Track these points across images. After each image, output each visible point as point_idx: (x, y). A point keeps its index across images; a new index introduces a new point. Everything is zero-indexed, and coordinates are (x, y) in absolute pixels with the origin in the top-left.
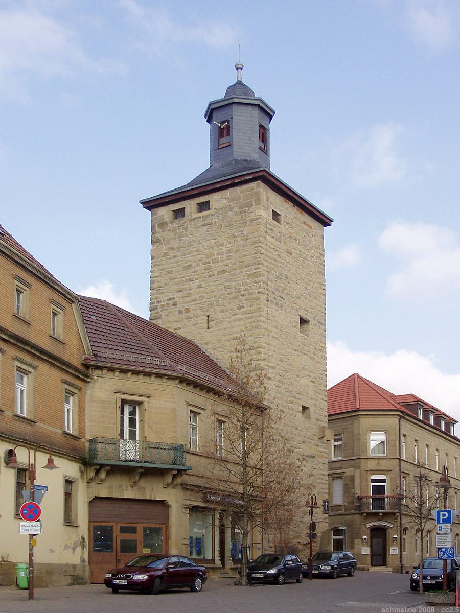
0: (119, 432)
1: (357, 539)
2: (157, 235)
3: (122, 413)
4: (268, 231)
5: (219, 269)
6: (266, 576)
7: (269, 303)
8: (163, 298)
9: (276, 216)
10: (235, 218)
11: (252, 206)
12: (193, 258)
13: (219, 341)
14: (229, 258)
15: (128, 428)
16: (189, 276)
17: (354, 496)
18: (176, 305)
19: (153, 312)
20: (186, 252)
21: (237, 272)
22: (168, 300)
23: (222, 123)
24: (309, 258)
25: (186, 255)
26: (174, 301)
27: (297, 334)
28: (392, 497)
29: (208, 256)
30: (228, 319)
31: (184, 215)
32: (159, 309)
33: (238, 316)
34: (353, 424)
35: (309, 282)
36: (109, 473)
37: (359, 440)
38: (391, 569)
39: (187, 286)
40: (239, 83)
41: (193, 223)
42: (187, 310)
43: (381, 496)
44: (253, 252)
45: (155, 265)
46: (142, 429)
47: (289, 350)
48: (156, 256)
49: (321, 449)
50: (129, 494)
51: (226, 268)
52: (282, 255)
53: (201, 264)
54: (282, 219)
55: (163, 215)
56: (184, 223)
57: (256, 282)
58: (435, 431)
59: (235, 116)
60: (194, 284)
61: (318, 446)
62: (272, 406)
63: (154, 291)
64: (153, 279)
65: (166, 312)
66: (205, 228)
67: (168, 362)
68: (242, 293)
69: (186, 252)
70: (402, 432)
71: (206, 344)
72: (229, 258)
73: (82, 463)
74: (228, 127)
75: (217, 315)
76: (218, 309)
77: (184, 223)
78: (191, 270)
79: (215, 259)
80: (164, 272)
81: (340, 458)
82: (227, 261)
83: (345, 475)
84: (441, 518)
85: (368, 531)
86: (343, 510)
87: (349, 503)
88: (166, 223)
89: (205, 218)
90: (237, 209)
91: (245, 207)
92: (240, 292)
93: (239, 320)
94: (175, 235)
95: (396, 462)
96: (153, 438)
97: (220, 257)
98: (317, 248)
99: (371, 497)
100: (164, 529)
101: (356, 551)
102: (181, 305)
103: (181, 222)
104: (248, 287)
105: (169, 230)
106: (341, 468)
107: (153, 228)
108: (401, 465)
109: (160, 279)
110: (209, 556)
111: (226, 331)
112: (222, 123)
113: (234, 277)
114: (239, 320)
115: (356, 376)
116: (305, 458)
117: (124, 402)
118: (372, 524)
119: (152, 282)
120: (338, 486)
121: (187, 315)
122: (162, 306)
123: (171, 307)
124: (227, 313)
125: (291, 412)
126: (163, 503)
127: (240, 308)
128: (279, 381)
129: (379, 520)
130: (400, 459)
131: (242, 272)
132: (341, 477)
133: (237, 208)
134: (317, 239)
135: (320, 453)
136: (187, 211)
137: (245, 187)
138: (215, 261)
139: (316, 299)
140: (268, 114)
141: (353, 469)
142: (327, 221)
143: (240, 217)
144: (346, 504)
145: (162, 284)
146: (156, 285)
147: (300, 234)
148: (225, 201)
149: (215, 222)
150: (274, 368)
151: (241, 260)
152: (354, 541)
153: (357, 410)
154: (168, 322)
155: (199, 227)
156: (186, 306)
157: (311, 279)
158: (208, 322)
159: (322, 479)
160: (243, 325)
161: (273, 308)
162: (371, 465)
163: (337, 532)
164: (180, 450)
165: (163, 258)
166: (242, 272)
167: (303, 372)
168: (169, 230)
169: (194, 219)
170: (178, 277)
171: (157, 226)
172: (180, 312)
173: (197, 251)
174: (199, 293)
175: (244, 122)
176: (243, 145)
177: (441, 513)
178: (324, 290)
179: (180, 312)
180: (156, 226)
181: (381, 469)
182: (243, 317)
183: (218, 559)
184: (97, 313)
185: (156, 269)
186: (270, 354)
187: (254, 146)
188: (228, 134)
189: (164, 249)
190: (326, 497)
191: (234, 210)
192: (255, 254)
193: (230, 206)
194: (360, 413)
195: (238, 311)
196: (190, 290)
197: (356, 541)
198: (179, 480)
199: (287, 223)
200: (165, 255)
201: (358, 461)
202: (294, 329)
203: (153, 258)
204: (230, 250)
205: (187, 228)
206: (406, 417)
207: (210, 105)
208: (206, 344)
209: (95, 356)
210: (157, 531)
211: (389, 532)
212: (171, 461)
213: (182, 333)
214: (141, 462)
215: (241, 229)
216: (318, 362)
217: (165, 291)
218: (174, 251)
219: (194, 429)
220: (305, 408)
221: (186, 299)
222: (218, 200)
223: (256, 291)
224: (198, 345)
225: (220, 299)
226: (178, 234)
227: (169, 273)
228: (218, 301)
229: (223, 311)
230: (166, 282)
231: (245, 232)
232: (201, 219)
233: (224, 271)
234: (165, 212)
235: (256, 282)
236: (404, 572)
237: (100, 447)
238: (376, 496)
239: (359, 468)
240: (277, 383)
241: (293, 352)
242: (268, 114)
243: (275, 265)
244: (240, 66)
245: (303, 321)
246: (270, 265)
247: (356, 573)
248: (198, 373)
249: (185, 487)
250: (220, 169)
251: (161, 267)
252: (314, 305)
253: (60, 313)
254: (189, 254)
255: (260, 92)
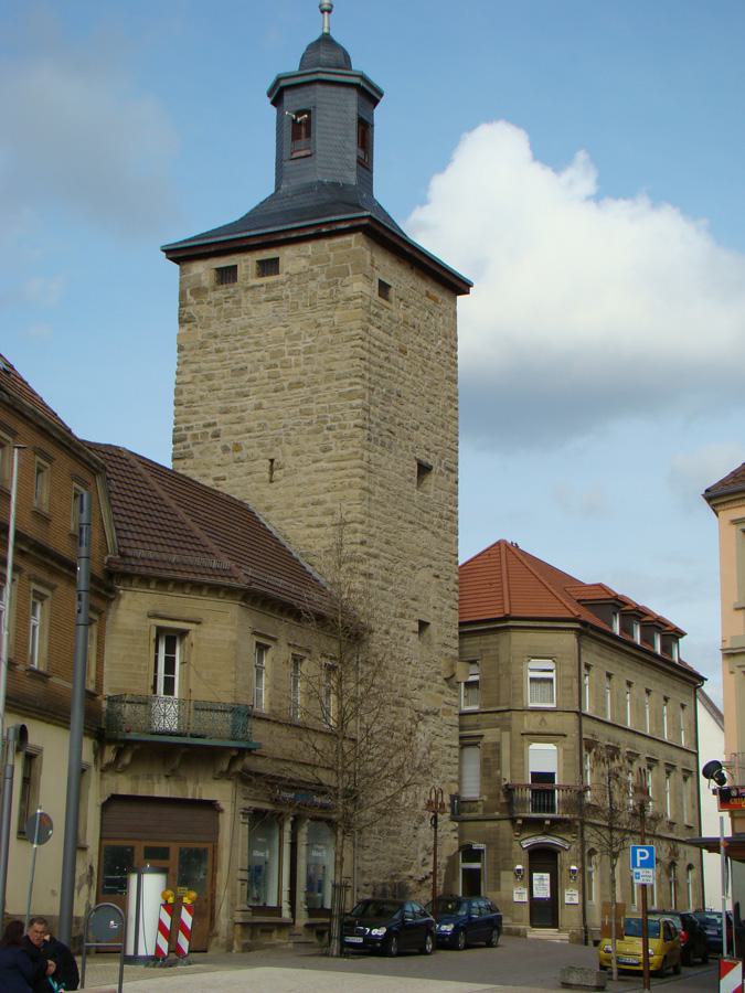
0: (152, 683)
1: (504, 870)
2: (189, 309)
3: (157, 650)
4: (372, 317)
5: (294, 379)
6: (369, 939)
7: (372, 443)
8: (197, 423)
9: (384, 288)
10: (320, 293)
11: (348, 275)
12: (249, 355)
13: (289, 506)
14: (308, 361)
15: (163, 675)
16: (241, 387)
17: (500, 784)
18: (218, 436)
19: (179, 445)
20: (238, 345)
21: (321, 387)
22: (205, 426)
23: (299, 113)
24: (433, 354)
25: (236, 349)
26: (215, 428)
27: (413, 492)
28: (568, 788)
29: (274, 355)
30: (304, 468)
31: (235, 279)
32: (189, 442)
33: (322, 463)
34: (497, 643)
35: (432, 398)
36: (136, 758)
37: (508, 674)
38: (565, 936)
39: (238, 405)
40: (326, 40)
41: (250, 294)
42: (237, 447)
43: (547, 786)
44: (348, 355)
45: (185, 362)
46: (185, 676)
47: (400, 523)
48: (187, 346)
49: (447, 699)
50: (162, 789)
51: (303, 378)
52: (393, 357)
53: (262, 368)
54: (392, 293)
55: (200, 275)
56: (236, 292)
57: (352, 408)
58: (643, 655)
59: (326, 103)
60: (252, 401)
61: (442, 693)
62: (375, 626)
63: (181, 408)
64: (181, 387)
65: (201, 447)
66: (270, 305)
67: (227, 564)
68: (329, 424)
69: (238, 345)
70: (584, 660)
71: (268, 509)
72: (308, 361)
73: (96, 738)
74: (308, 123)
75: (285, 455)
76: (289, 449)
77: (236, 292)
78: (247, 377)
79: (285, 361)
80: (198, 374)
81: (475, 708)
82: (306, 367)
83: (485, 740)
84: (639, 858)
85: (525, 856)
86: (481, 810)
87: (491, 796)
88: (205, 290)
89: (269, 287)
90: (322, 278)
91: (336, 276)
92: (325, 422)
93: (323, 471)
94: (220, 311)
95: (572, 718)
96: (202, 694)
97: (293, 358)
98: (446, 337)
99: (527, 786)
100: (210, 852)
101: (503, 894)
102: (227, 438)
103: (232, 290)
104: (338, 414)
105: (209, 303)
106: (477, 727)
107: (182, 295)
108: (583, 726)
109: (192, 387)
110: (272, 903)
111: (301, 490)
112: (299, 113)
113: (316, 396)
114: (323, 471)
115: (503, 546)
116: (422, 716)
117: (160, 630)
118: (532, 841)
119: (178, 392)
120: (473, 759)
121: (237, 455)
122: (195, 436)
123: (210, 439)
124: (304, 457)
125: (401, 633)
126: (211, 806)
127: (325, 450)
128: (384, 579)
129: (545, 834)
130: (580, 715)
131: (328, 388)
132: (475, 745)
133: (324, 275)
134: (447, 318)
135: (446, 706)
136: (241, 272)
137: (337, 241)
138: (284, 365)
139: (443, 426)
140: (369, 95)
141: (498, 730)
142: (460, 285)
143: (328, 291)
144: (485, 798)
145: (195, 397)
146: (185, 397)
147: (419, 316)
148: (303, 262)
149: (287, 297)
150: (376, 557)
151: (327, 366)
152: (499, 874)
153: (506, 618)
154: (204, 471)
155: (260, 303)
156: (236, 439)
157: (436, 393)
158: (272, 470)
159: (449, 755)
160: (328, 481)
161: (376, 451)
162: (530, 723)
163: (470, 854)
164: (245, 714)
165: (198, 352)
166: (328, 388)
167: (421, 559)
168: (209, 303)
169: (253, 287)
170: (224, 386)
171: (190, 294)
172: (225, 449)
173: (257, 343)
174: (257, 419)
175: (334, 112)
176: (331, 159)
177: (638, 851)
178: (456, 409)
179: (225, 449)
180: (188, 292)
181: (547, 731)
182: (330, 465)
183: (286, 906)
184: (101, 465)
185: (186, 369)
186: (373, 531)
187: (349, 157)
188: (308, 134)
189: (200, 334)
190: (455, 788)
191: (319, 279)
192: (351, 358)
193: (312, 270)
194: (511, 623)
195: (321, 455)
196: (243, 411)
197: (504, 875)
198: (238, 767)
199: (401, 300)
200: (203, 345)
201: (507, 714)
202: (409, 485)
203: (181, 349)
204: (310, 347)
205: (239, 302)
206: (591, 632)
207: (279, 80)
208: (268, 509)
209: (123, 555)
210: (199, 855)
211: (563, 857)
212: (228, 734)
213: (225, 488)
214: (185, 736)
215: (329, 313)
216: (445, 540)
217: (200, 409)
218: (218, 340)
219: (259, 674)
220: (423, 625)
221: (237, 427)
222: (292, 259)
223: (352, 423)
224: (254, 510)
225: (292, 433)
226: (225, 310)
227: (209, 378)
228: (289, 435)
229: (296, 454)
230: (202, 393)
231: (336, 319)
232: (264, 289)
233: (299, 384)
234: (203, 270)
235: (352, 408)
236: (590, 942)
237: (127, 709)
238: (537, 786)
239: (508, 728)
240: (380, 583)
241: (406, 525)
242: (369, 95)
243: (379, 375)
244: (326, 7)
245: (424, 469)
246: (374, 378)
247: (502, 940)
248: (283, 597)
249: (246, 778)
250: (295, 198)
251: (194, 367)
252: (439, 437)
253: (46, 468)
254: (243, 348)
255: (363, 63)
